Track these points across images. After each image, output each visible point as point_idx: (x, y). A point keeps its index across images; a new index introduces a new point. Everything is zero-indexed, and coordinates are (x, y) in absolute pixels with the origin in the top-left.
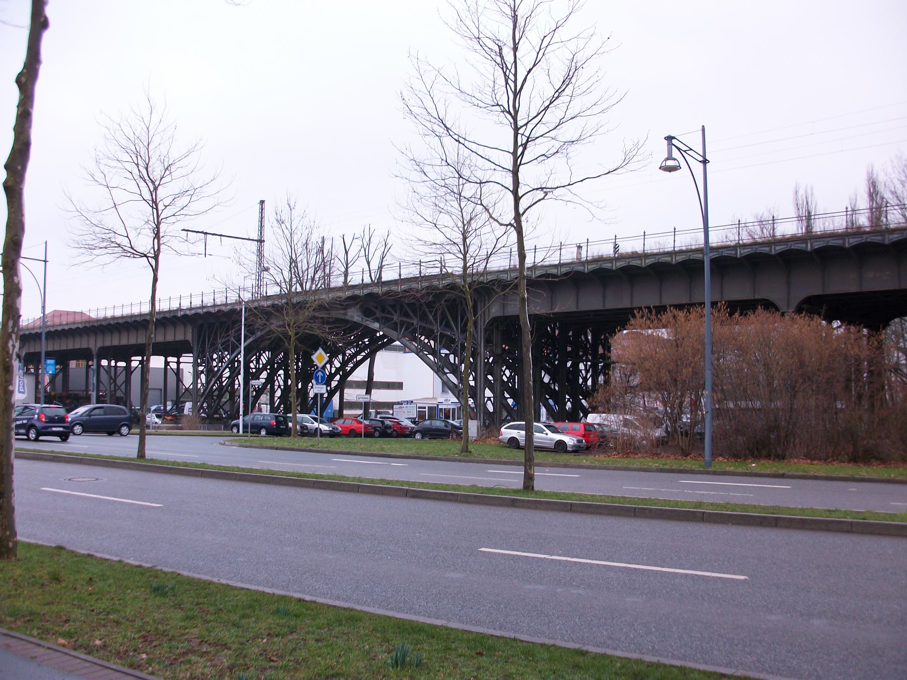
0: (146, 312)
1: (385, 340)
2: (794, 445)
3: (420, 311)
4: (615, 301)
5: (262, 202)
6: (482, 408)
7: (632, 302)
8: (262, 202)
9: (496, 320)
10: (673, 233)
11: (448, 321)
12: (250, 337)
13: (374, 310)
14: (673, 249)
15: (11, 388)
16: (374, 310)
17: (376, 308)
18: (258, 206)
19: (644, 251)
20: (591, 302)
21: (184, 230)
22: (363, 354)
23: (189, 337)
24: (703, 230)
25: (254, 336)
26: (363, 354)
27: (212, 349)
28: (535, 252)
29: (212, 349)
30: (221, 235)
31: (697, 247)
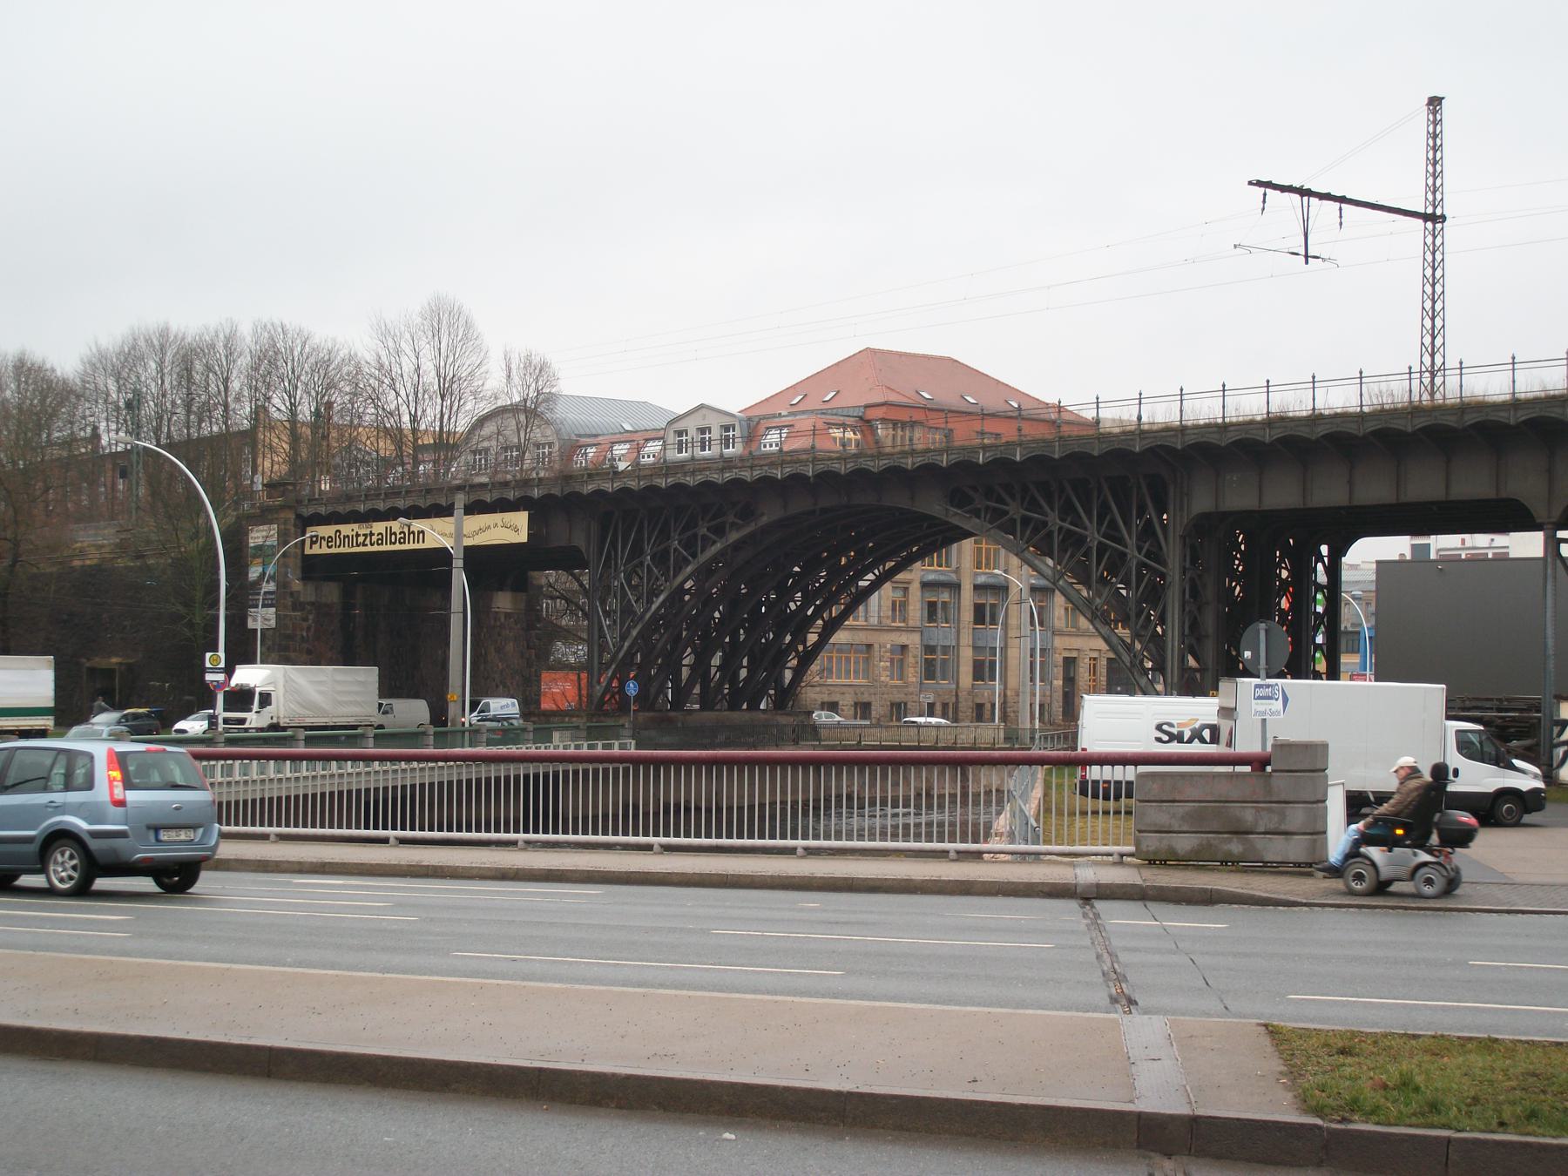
1: (914, 549)
2: (1528, 710)
3: (1060, 498)
4: (1330, 491)
5: (1435, 102)
7: (1447, 487)
8: (1435, 102)
9: (1205, 516)
10: (1095, 406)
11: (1113, 523)
12: (714, 542)
13: (971, 493)
14: (1359, 409)
15: (1289, 676)
16: (971, 493)
17: (975, 489)
18: (1422, 114)
19: (1514, 393)
20: (1282, 493)
21: (1259, 184)
22: (870, 576)
23: (579, 541)
24: (1565, 362)
25: (724, 540)
26: (870, 576)
27: (630, 567)
28: (1514, 370)
29: (630, 567)
30: (1343, 200)
31: (1241, 419)
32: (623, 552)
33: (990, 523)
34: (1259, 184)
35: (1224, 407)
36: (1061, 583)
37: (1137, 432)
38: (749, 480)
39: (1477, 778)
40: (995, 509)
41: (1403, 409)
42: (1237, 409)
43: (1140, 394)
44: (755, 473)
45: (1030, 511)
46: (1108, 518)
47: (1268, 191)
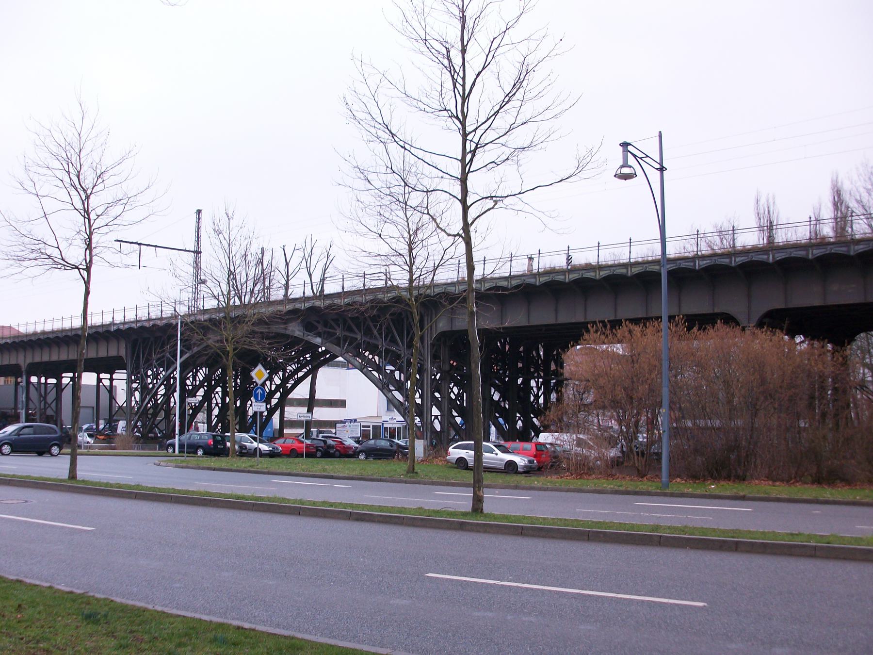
0: (78, 327)
1: (328, 356)
4: (568, 315)
5: (199, 212)
6: (429, 427)
8: (199, 212)
9: (443, 334)
10: (629, 244)
11: (393, 337)
12: (186, 353)
16: (316, 324)
17: (318, 322)
22: (305, 370)
25: (191, 352)
26: (305, 370)
30: (156, 246)
31: (654, 258)
32: (143, 357)
33: (326, 339)
34: (117, 241)
35: (630, 252)
36: (365, 370)
37: (598, 267)
38: (136, 327)
39: (686, 437)
40: (329, 332)
41: (763, 247)
42: (684, 248)
43: (630, 240)
44: (138, 325)
45: (394, 325)
46: (390, 336)
47: (122, 243)
